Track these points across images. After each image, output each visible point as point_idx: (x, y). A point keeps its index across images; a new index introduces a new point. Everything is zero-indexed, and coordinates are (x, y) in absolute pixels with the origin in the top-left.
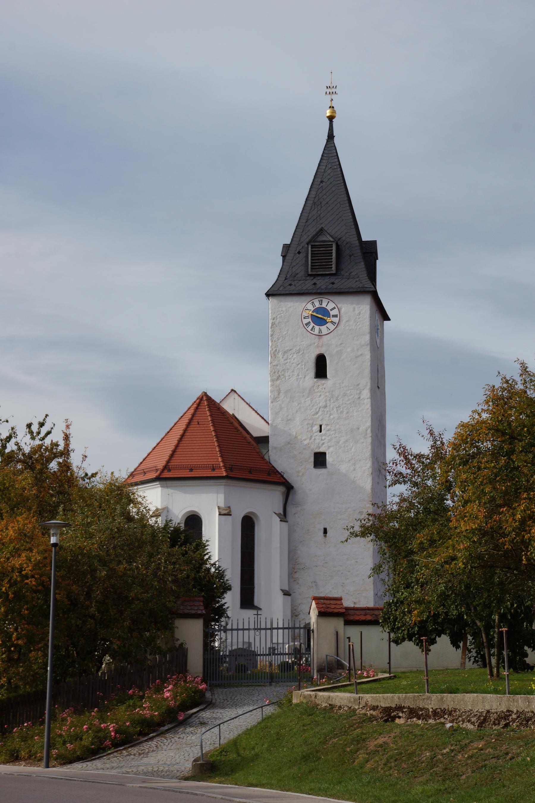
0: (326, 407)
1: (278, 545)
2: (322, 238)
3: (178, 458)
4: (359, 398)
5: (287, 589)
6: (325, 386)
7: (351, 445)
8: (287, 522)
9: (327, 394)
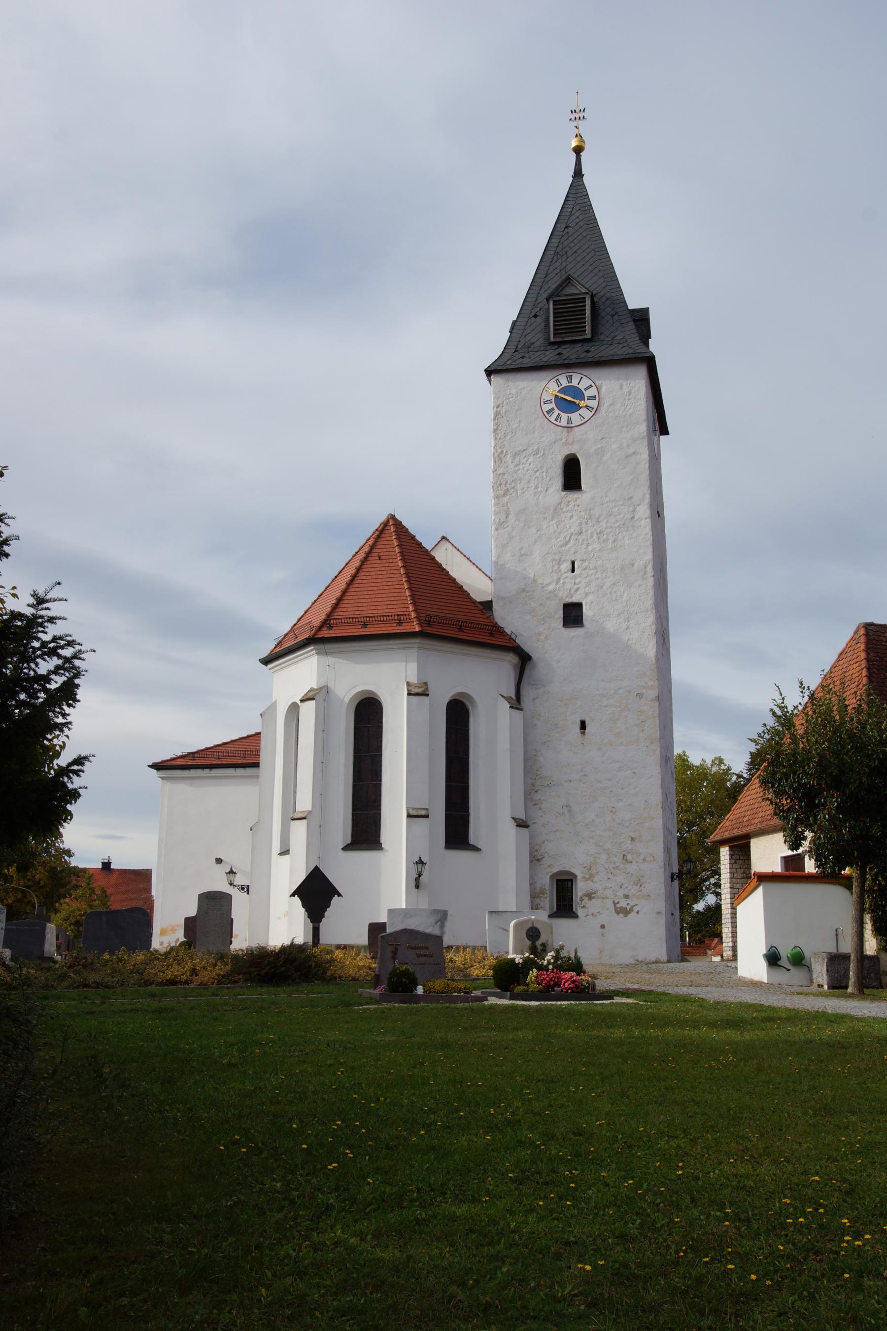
0: (580, 533)
1: (508, 746)
2: (570, 290)
3: (345, 609)
4: (633, 518)
5: (523, 817)
6: (578, 502)
7: (622, 590)
8: (521, 709)
9: (583, 514)
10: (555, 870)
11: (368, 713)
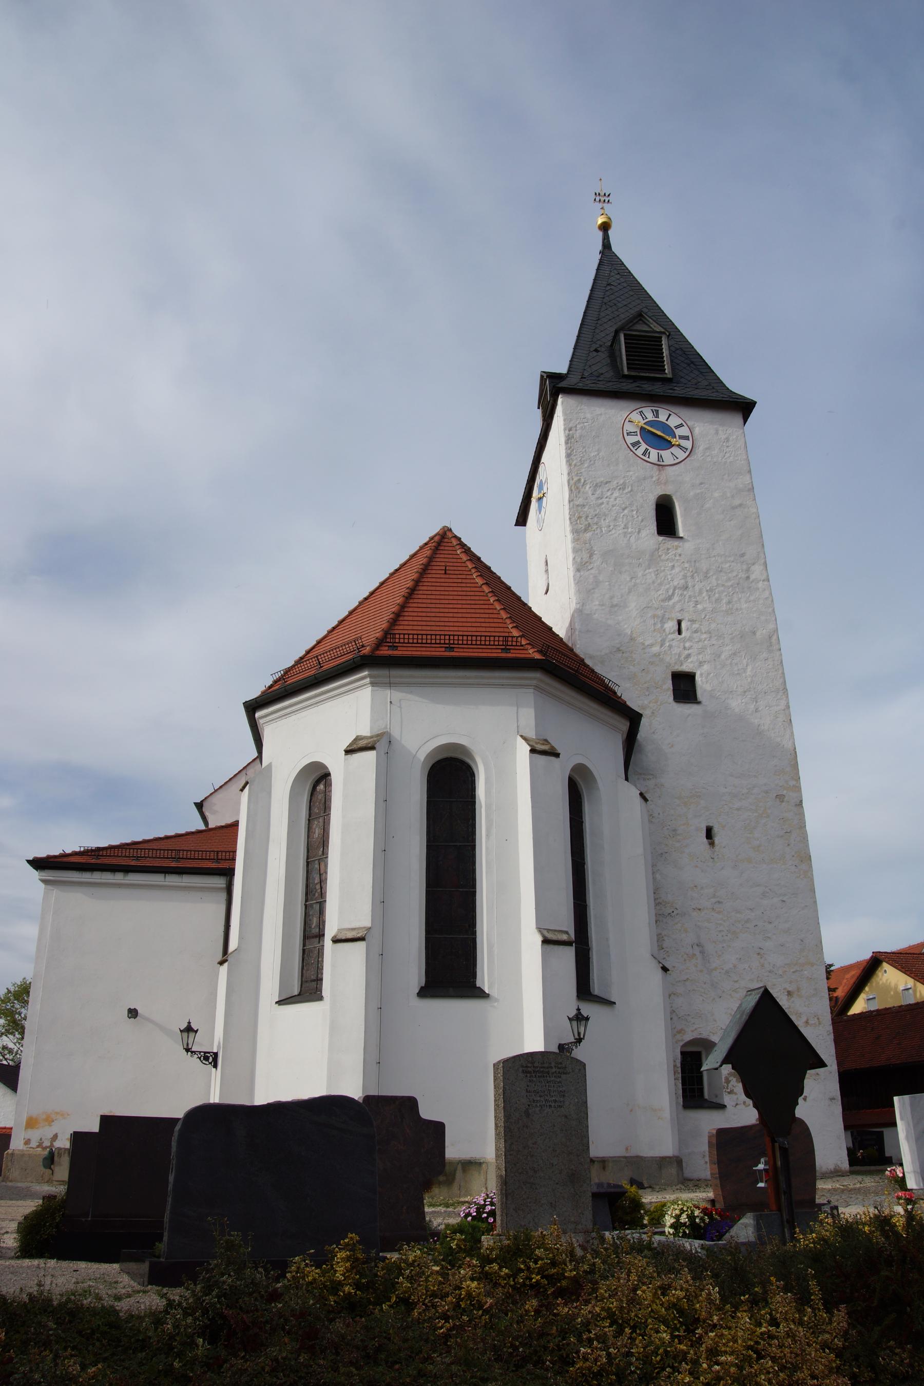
0: (686, 588)
2: (641, 327)
4: (748, 578)
6: (679, 551)
7: (745, 661)
10: (688, 1037)
11: (451, 783)
